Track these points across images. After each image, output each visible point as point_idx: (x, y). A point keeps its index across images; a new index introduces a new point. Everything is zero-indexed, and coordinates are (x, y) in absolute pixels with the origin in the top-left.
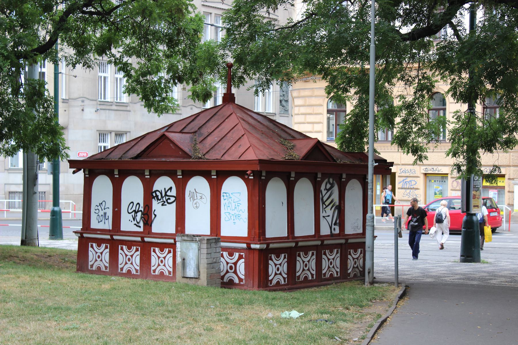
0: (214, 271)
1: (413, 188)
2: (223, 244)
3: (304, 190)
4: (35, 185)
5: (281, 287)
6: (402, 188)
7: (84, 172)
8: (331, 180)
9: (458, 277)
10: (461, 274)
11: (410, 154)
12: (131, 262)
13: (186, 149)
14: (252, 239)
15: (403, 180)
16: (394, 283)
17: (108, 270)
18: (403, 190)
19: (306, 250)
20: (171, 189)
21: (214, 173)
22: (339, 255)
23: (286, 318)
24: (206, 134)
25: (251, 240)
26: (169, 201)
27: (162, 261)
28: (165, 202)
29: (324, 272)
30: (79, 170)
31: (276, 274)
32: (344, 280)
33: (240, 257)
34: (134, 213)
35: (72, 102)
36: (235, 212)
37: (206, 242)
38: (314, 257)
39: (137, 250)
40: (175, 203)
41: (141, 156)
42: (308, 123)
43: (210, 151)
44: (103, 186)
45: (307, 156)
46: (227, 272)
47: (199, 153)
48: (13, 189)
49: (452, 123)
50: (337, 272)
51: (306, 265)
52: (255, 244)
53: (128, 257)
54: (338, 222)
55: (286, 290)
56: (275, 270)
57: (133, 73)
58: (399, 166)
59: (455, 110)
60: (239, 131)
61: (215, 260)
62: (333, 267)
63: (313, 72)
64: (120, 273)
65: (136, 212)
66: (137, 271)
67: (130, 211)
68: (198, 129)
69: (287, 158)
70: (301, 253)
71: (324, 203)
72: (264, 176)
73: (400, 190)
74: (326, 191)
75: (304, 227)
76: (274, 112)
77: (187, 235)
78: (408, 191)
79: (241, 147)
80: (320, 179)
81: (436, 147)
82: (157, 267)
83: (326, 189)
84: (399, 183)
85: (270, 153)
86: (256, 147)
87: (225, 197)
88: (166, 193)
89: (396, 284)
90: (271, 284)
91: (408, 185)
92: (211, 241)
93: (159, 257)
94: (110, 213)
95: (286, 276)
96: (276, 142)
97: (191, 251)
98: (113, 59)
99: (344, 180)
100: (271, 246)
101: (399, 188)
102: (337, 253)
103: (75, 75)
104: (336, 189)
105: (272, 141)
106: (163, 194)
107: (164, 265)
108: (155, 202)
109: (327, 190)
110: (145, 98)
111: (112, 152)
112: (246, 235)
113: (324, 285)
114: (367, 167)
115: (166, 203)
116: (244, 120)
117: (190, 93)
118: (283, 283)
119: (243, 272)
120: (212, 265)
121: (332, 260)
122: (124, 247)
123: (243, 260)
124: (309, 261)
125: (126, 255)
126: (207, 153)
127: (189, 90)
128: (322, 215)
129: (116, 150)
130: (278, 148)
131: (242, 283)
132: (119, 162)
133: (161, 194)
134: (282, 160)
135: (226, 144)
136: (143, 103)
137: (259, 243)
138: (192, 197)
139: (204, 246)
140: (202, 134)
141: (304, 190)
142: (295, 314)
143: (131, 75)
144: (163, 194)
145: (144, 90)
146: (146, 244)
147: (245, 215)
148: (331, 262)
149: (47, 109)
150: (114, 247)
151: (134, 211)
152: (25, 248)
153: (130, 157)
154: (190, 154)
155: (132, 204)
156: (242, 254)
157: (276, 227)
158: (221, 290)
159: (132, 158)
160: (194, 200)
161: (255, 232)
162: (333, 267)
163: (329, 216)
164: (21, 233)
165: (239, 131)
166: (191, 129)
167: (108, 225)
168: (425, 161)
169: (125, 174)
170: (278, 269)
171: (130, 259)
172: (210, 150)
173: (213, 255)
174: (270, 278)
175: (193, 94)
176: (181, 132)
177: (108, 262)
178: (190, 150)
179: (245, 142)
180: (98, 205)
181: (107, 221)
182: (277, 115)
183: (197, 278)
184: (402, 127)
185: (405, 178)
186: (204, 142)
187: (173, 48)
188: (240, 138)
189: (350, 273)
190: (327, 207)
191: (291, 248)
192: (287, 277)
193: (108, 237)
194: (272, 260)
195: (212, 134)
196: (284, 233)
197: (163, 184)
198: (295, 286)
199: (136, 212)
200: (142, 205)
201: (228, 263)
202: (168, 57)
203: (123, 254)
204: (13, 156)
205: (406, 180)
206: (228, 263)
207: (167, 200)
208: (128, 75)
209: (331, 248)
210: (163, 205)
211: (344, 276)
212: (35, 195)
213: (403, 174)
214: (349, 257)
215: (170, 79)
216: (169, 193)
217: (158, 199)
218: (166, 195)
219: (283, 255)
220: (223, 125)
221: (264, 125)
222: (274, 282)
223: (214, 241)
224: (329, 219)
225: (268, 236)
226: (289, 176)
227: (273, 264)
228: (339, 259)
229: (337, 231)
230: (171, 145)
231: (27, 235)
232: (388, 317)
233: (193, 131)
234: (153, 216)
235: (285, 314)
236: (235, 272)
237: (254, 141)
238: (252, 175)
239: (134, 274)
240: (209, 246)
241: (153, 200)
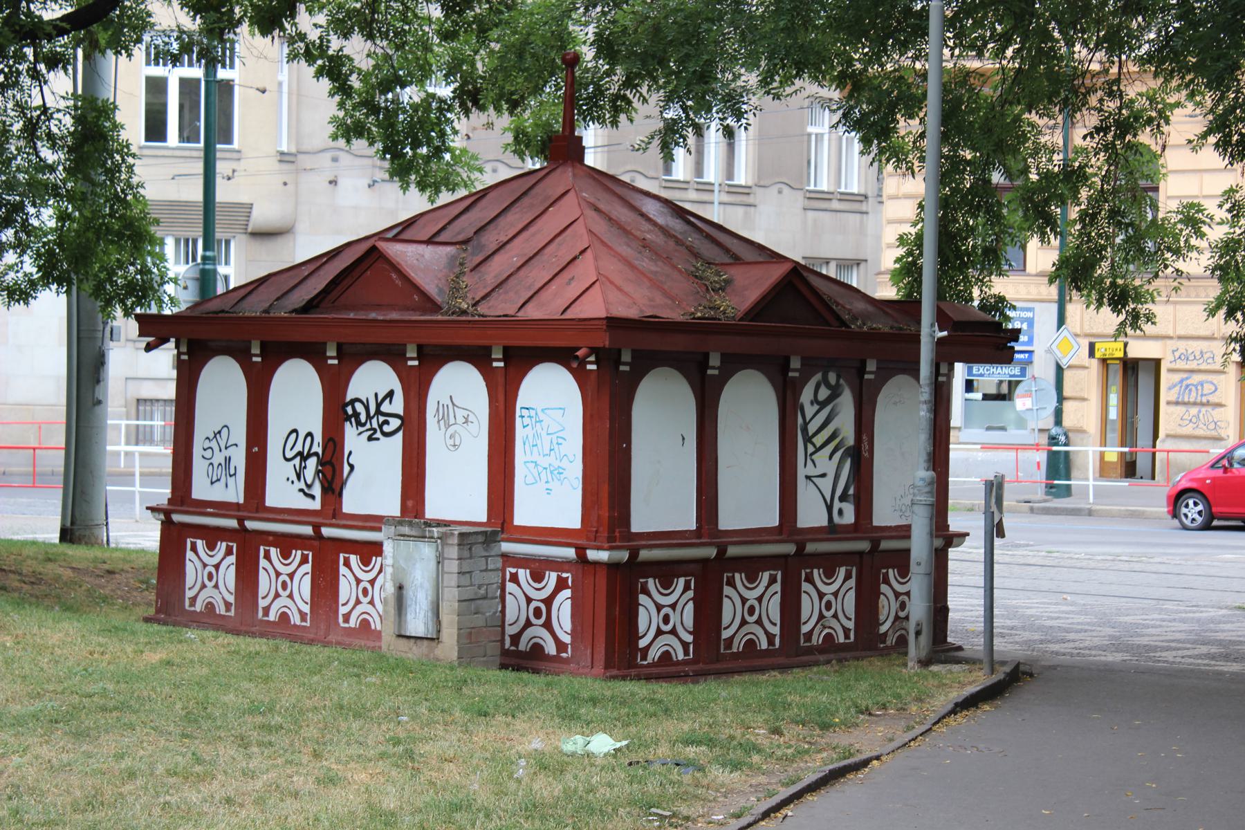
0: (479, 621)
1: (1208, 404)
2: (507, 547)
3: (749, 407)
4: (98, 381)
5: (673, 669)
6: (1177, 403)
7: (177, 347)
8: (832, 378)
9: (1204, 649)
10: (1220, 643)
11: (1106, 310)
13: (431, 288)
14: (592, 536)
15: (1181, 381)
16: (981, 661)
17: (232, 613)
18: (1180, 410)
19: (752, 567)
20: (390, 394)
21: (497, 354)
22: (852, 582)
23: (573, 755)
24: (493, 247)
25: (588, 539)
26: (386, 429)
27: (365, 592)
28: (375, 431)
29: (805, 629)
30: (162, 341)
31: (659, 632)
32: (863, 653)
33: (561, 585)
34: (298, 460)
35: (304, 161)
36: (551, 460)
37: (455, 541)
38: (777, 587)
39: (304, 560)
40: (400, 434)
41: (317, 306)
43: (494, 294)
44: (223, 383)
45: (760, 310)
46: (528, 624)
47: (464, 298)
48: (148, 391)
49: (1222, 223)
50: (846, 631)
51: (751, 611)
52: (599, 548)
53: (281, 579)
54: (851, 491)
55: (687, 675)
56: (656, 620)
57: (355, 81)
58: (1169, 342)
59: (1227, 187)
60: (578, 239)
61: (482, 591)
62: (835, 616)
64: (262, 621)
65: (303, 457)
66: (303, 616)
67: (289, 455)
68: (475, 233)
69: (699, 314)
70: (737, 576)
71: (808, 440)
72: (625, 364)
73: (1173, 408)
74: (816, 407)
75: (749, 503)
76: (862, 192)
77: (429, 524)
78: (1194, 410)
79: (573, 284)
80: (796, 374)
81: (1176, 289)
82: (354, 608)
83: (815, 401)
84: (1170, 389)
85: (651, 300)
86: (611, 283)
87: (527, 421)
88: (378, 405)
89: (986, 667)
90: (644, 657)
91: (1194, 394)
92: (472, 539)
93: (358, 581)
94: (239, 458)
95: (689, 638)
96: (680, 271)
97: (418, 565)
98: (302, 45)
99: (872, 377)
100: (644, 554)
101: (1168, 403)
102: (848, 577)
103: (261, 86)
104: (846, 403)
105: (667, 269)
106: (372, 411)
107: (291, 596)
108: (350, 431)
109: (818, 403)
110: (392, 150)
111: (251, 292)
112: (577, 524)
113: (803, 666)
114: (916, 339)
115: (378, 435)
116: (597, 209)
117: (509, 138)
118: (681, 656)
119: (568, 626)
120: (473, 605)
121: (832, 598)
122: (273, 551)
123: (567, 593)
124: (760, 599)
125: (278, 574)
126: (483, 298)
127: (505, 130)
128: (801, 472)
129: (261, 288)
130: (681, 286)
131: (564, 655)
132: (264, 322)
133: (367, 408)
134: (681, 319)
135: (537, 275)
136: (387, 164)
137: (606, 545)
138: (444, 420)
139: (453, 552)
140: (481, 247)
141: (749, 407)
142: (602, 744)
143: (351, 87)
144: (372, 411)
145: (389, 124)
146: (329, 545)
147: (575, 469)
148: (829, 602)
149: (113, 175)
150: (248, 550)
151: (300, 454)
152: (73, 551)
153: (291, 307)
154: (439, 299)
155: (294, 435)
156: (565, 575)
157: (662, 500)
158: (501, 674)
159: (295, 311)
160: (448, 426)
161: (599, 516)
162: (835, 616)
163: (823, 475)
164: (60, 510)
165: (578, 239)
166: (459, 233)
167: (234, 492)
168: (1148, 328)
169: (277, 353)
170: (666, 620)
171: (287, 586)
172: (493, 290)
173: (478, 578)
174: (642, 643)
175: (516, 138)
176: (429, 242)
177: (233, 590)
178: (441, 291)
179: (585, 271)
180: (211, 436)
181: (231, 481)
182: (870, 200)
183: (432, 639)
184: (1081, 234)
185: (1185, 375)
186: (483, 268)
187: (460, 13)
188: (575, 258)
189: (886, 634)
190: (818, 450)
191: (704, 561)
193: (233, 523)
194: (649, 594)
195: (508, 246)
196: (689, 522)
197: (373, 381)
198: (718, 666)
199: (303, 457)
200: (318, 438)
201: (529, 600)
202: (446, 36)
203: (271, 566)
204: (27, 303)
205: (1188, 382)
206: (529, 600)
207: (381, 426)
208: (342, 88)
209: (829, 563)
210: (370, 439)
211: (869, 641)
212: (97, 408)
213: (1181, 365)
214: (884, 588)
215: (454, 98)
216: (385, 408)
217: (359, 424)
218: (378, 412)
219: (682, 581)
220: (540, 223)
221: (655, 224)
222: (654, 654)
223: (481, 539)
224: (826, 485)
225: (636, 527)
226: (704, 364)
227: (631, 605)
228: (852, 593)
229: (849, 517)
230: (394, 276)
231: (77, 514)
232: (878, 758)
233: (460, 238)
234: (346, 469)
235: (573, 743)
236: (548, 625)
237: (612, 268)
238: (592, 358)
239: (295, 625)
240: (466, 554)
241: (347, 424)
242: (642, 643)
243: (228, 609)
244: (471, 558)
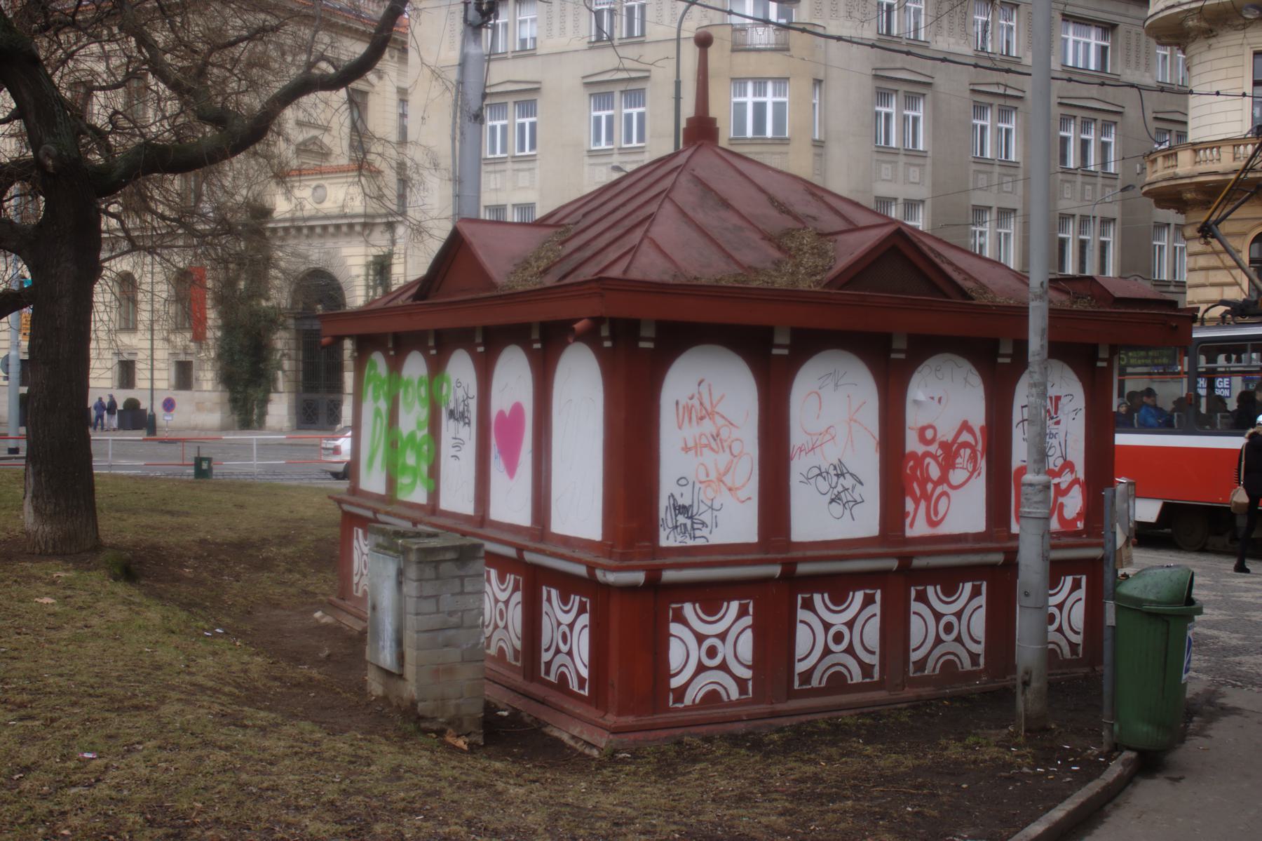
12: (832, 632)
17: (586, 693)
31: (701, 668)
42: (1213, 285)
56: (725, 651)
70: (930, 590)
95: (746, 674)
120: (441, 637)
135: (612, 254)
141: (415, 366)
170: (712, 652)
192: (754, 678)
194: (684, 622)
242: (675, 683)
243: (581, 687)
244: (437, 578)
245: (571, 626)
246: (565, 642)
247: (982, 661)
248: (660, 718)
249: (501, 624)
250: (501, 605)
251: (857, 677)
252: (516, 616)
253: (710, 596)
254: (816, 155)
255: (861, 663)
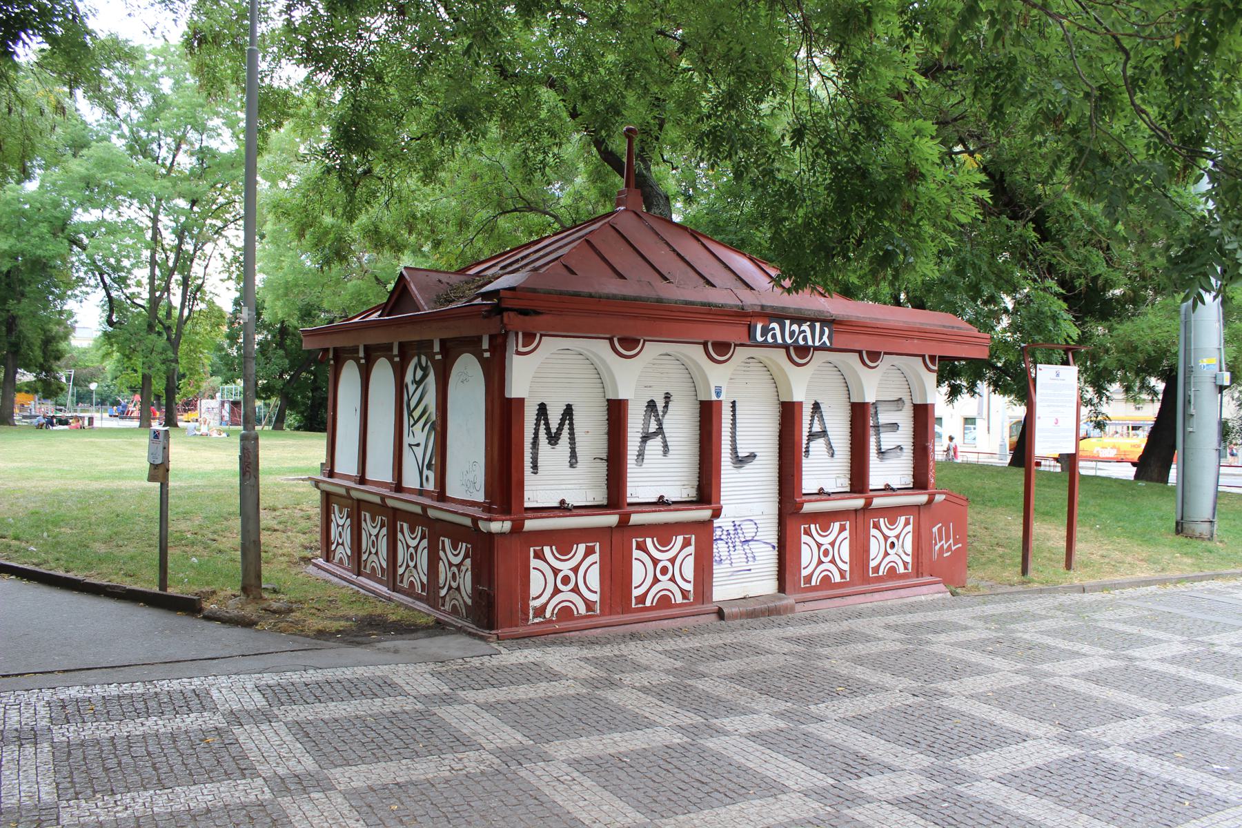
12: (822, 549)
50: (905, 564)
51: (826, 553)
63: (894, 186)
71: (410, 414)
83: (414, 381)
104: (431, 379)
124: (832, 544)
141: (383, 374)
163: (418, 445)
190: (416, 422)
224: (419, 451)
229: (430, 486)
245: (416, 548)
246: (454, 574)
247: (910, 566)
248: (521, 630)
249: (374, 551)
250: (411, 550)
251: (837, 579)
252: (423, 559)
253: (564, 541)
254: (105, 334)
255: (840, 570)
